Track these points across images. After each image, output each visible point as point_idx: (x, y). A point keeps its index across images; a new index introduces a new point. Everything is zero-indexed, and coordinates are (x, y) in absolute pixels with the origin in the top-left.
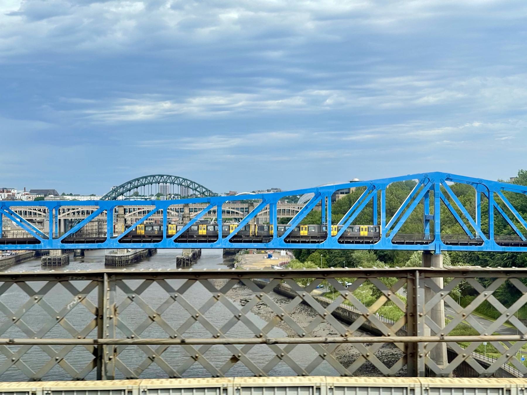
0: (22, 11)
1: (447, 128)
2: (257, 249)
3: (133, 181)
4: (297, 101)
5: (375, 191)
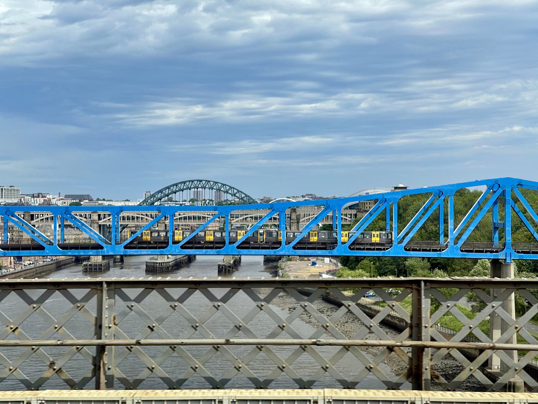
0: (54, 14)
1: (486, 132)
2: (300, 256)
3: (171, 186)
4: (330, 105)
5: (442, 198)
